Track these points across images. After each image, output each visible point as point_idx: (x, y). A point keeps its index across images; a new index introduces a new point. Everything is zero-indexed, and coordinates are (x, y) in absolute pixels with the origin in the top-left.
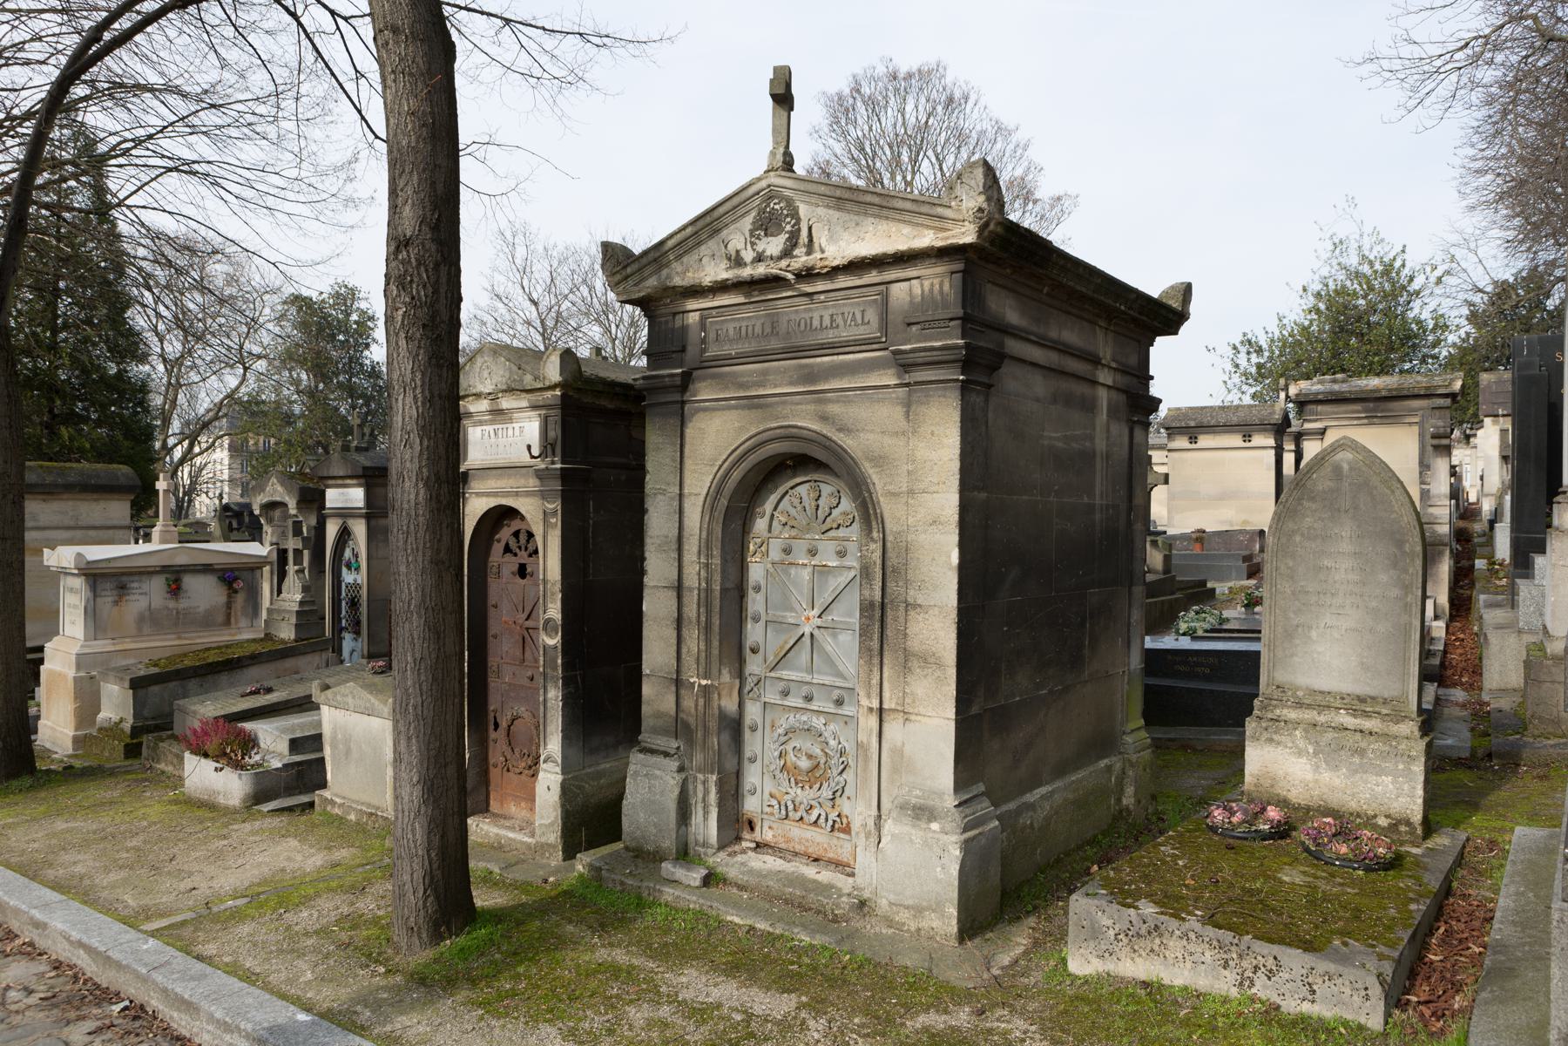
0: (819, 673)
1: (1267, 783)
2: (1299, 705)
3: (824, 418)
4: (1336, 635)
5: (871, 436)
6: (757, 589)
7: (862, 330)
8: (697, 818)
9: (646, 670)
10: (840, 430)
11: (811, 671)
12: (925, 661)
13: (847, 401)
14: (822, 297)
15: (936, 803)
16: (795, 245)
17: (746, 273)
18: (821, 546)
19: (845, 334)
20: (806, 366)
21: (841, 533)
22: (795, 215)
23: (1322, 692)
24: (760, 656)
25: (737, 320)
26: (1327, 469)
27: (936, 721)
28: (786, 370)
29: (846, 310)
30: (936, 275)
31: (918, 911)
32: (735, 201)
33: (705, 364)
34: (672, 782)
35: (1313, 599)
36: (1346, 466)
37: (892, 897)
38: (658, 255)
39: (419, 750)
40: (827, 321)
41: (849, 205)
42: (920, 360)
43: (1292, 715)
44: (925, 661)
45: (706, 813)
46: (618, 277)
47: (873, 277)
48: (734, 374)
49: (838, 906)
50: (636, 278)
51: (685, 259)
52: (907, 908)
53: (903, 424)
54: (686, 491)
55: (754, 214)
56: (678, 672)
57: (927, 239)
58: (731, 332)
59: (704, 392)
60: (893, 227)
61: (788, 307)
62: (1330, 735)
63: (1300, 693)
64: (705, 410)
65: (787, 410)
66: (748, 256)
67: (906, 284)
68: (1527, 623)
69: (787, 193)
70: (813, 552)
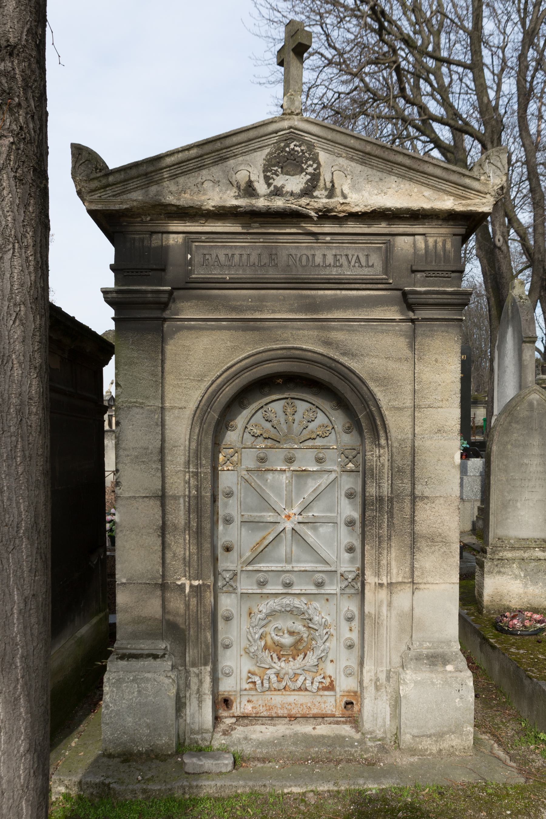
0: (298, 561)
1: (497, 599)
2: (513, 548)
3: (327, 343)
4: (531, 504)
5: (375, 361)
6: (229, 494)
7: (366, 271)
8: (191, 709)
9: (121, 577)
10: (344, 354)
11: (288, 560)
12: (433, 540)
13: (351, 330)
14: (328, 238)
15: (445, 649)
16: (315, 187)
17: (261, 203)
18: (298, 454)
19: (348, 273)
20: (308, 296)
21: (319, 442)
22: (315, 159)
23: (524, 539)
24: (234, 554)
25: (232, 251)
26: (525, 405)
27: (443, 586)
28: (285, 298)
29: (350, 253)
30: (440, 235)
31: (440, 736)
32: (252, 134)
33: (189, 286)
34: (167, 681)
35: (518, 483)
36: (535, 403)
37: (415, 731)
38: (148, 170)
39: (30, 711)
40: (330, 260)
41: (374, 162)
42: (431, 301)
43: (509, 555)
44: (433, 540)
45: (200, 701)
46: (95, 184)
47: (382, 227)
48: (225, 297)
49: (367, 751)
50: (118, 189)
51: (181, 180)
52: (430, 736)
53: (407, 352)
54: (167, 405)
55: (267, 151)
56: (163, 576)
57: (448, 203)
58: (222, 258)
59: (188, 311)
60: (415, 188)
61: (291, 245)
62: (533, 564)
63: (512, 541)
64: (190, 328)
65: (287, 334)
66: (261, 187)
67: (411, 238)
68: (467, 496)
69: (308, 138)
70: (290, 460)
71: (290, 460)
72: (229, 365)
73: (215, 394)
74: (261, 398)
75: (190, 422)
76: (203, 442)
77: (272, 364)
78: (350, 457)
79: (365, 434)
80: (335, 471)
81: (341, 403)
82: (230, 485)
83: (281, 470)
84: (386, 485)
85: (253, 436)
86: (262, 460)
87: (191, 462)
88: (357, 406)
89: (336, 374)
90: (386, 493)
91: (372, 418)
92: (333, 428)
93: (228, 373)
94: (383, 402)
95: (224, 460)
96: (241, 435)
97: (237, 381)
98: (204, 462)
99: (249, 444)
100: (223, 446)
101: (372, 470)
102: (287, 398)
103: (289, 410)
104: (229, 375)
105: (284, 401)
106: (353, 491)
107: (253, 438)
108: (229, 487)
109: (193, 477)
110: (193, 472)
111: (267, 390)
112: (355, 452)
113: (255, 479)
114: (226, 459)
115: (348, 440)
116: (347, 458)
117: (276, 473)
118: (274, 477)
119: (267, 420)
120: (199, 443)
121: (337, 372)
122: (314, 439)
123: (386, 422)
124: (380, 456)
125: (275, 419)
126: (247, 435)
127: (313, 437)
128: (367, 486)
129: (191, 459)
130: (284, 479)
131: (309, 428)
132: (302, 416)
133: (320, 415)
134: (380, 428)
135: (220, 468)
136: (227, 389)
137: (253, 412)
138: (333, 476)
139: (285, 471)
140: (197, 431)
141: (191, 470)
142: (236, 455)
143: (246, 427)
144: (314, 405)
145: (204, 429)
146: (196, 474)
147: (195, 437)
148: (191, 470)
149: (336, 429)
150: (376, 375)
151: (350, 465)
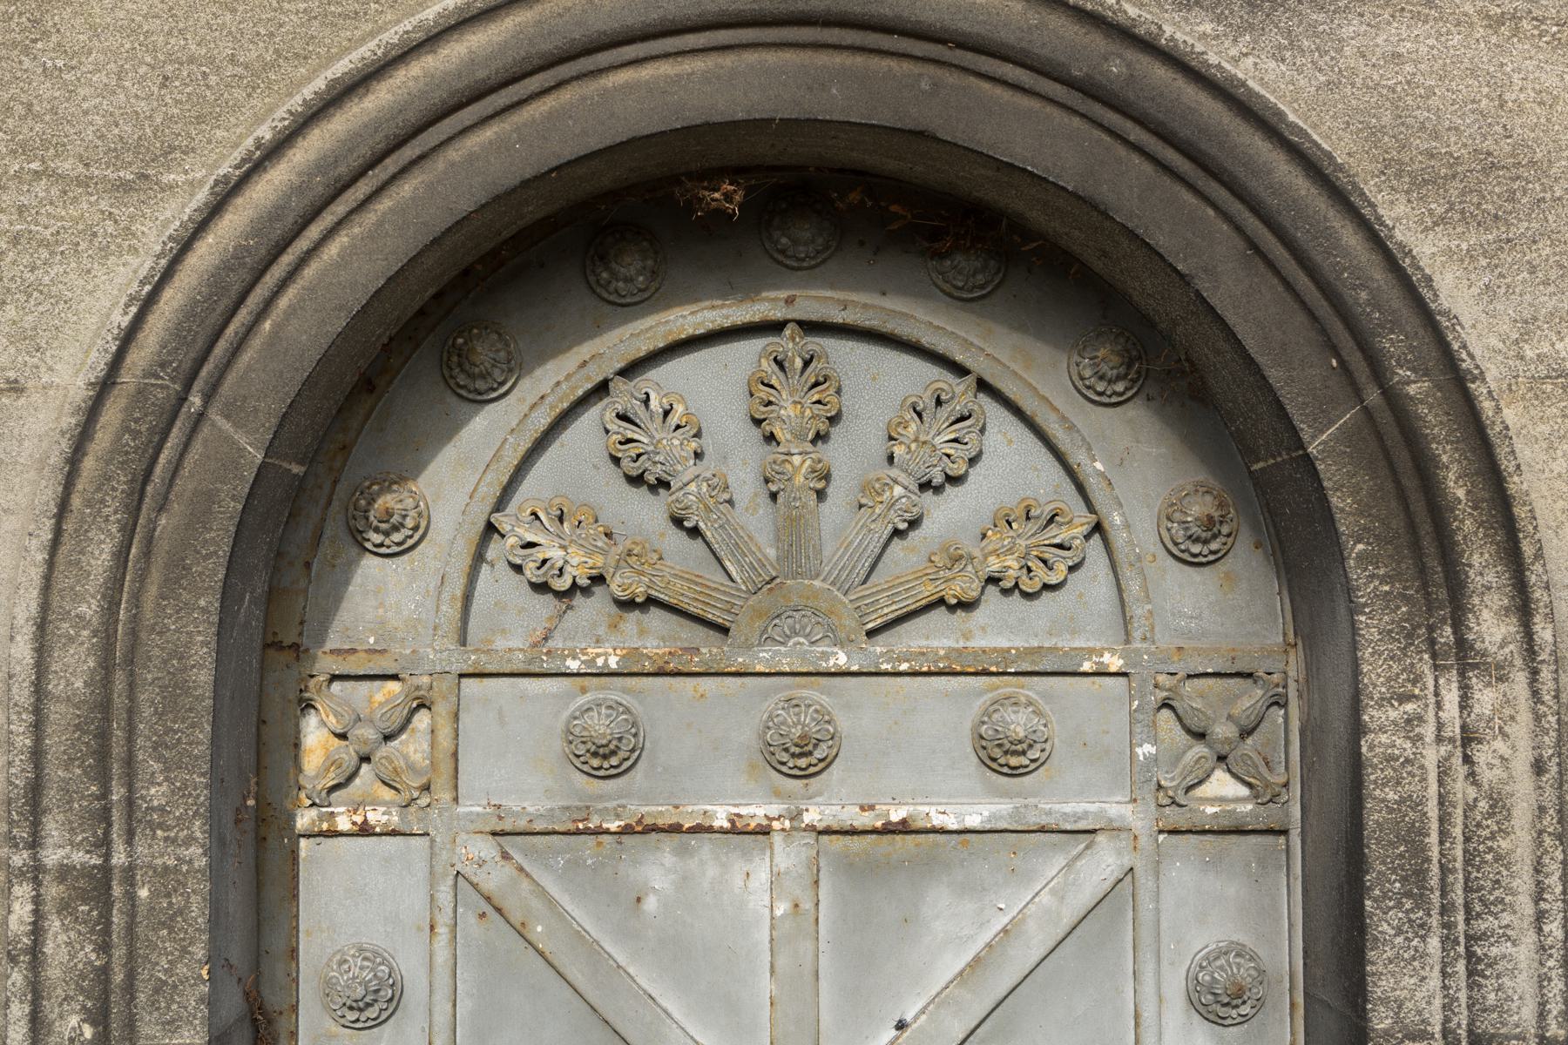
18: (858, 713)
21: (997, 628)
71: (801, 758)
72: (342, 67)
73: (236, 283)
74: (598, 328)
75: (48, 494)
76: (154, 647)
77: (665, 68)
78: (1223, 730)
79: (1356, 575)
80: (1115, 829)
81: (1160, 350)
82: (376, 937)
83: (736, 829)
84: (1524, 953)
85: (541, 588)
86: (606, 758)
87: (51, 796)
88: (1296, 376)
89: (1136, 133)
90: (1528, 1013)
91: (1403, 458)
92: (1098, 528)
93: (339, 125)
94: (1482, 330)
95: (332, 763)
96: (457, 587)
97: (406, 189)
98: (156, 794)
99: (512, 644)
100: (326, 664)
101: (1413, 837)
102: (773, 327)
103: (791, 411)
104: (350, 142)
105: (757, 344)
106: (1244, 972)
107: (546, 604)
108: (371, 956)
109: (64, 907)
110: (64, 872)
111: (632, 266)
112: (1250, 699)
113: (559, 894)
114: (348, 754)
115: (1212, 609)
116: (1200, 736)
117: (704, 847)
118: (685, 881)
119: (636, 480)
120: (118, 653)
121: (1140, 121)
122: (966, 606)
123: (1515, 485)
124: (1468, 738)
125: (690, 469)
126: (495, 584)
127: (957, 589)
128: (1378, 960)
129: (56, 773)
130: (756, 887)
131: (927, 527)
132: (878, 447)
133: (1003, 439)
134: (1467, 524)
135: (305, 819)
136: (333, 250)
137: (542, 419)
138: (1102, 864)
139: (765, 831)
140: (100, 557)
141: (52, 856)
142: (422, 720)
143: (490, 529)
144: (960, 370)
145: (162, 548)
146: (96, 887)
147: (89, 608)
148: (52, 856)
149: (1119, 538)
150: (1421, 143)
151: (1222, 785)
